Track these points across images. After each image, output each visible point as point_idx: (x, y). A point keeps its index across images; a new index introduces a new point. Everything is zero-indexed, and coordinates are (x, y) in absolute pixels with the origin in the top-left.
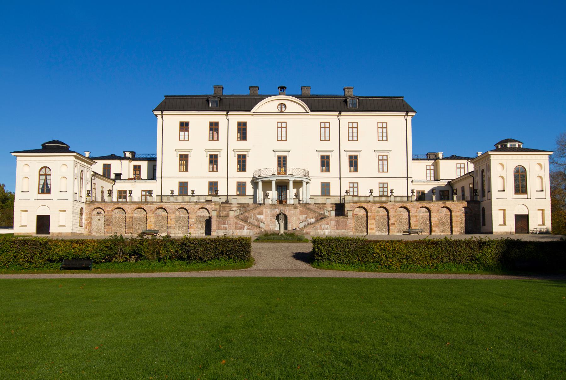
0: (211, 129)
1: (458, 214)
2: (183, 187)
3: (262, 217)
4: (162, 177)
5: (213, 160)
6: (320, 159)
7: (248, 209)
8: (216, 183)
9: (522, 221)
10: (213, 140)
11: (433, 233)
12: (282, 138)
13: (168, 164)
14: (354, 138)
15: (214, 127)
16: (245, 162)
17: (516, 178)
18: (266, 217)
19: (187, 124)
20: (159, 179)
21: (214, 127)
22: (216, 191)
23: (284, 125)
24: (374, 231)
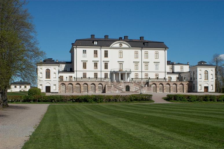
0: (95, 53)
1: (185, 86)
2: (85, 75)
3: (121, 87)
4: (101, 71)
5: (96, 65)
6: (82, 64)
8: (97, 73)
11: (178, 92)
12: (121, 57)
13: (78, 65)
14: (147, 57)
15: (96, 52)
17: (46, 72)
19: (85, 51)
21: (96, 52)
24: (158, 92)
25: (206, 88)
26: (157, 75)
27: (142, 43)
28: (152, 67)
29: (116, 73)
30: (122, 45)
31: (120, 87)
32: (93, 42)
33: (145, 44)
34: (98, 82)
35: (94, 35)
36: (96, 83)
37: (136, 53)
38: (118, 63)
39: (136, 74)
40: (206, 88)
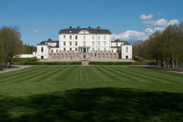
0: (70, 37)
5: (71, 43)
8: (71, 48)
10: (70, 39)
13: (61, 44)
14: (99, 39)
15: (71, 37)
16: (76, 44)
17: (42, 49)
19: (65, 36)
20: (60, 47)
21: (71, 37)
22: (71, 49)
25: (127, 57)
26: (105, 49)
27: (97, 31)
28: (102, 44)
29: (81, 48)
30: (85, 32)
31: (81, 56)
32: (69, 31)
33: (98, 31)
34: (69, 53)
35: (90, 27)
36: (64, 54)
37: (93, 37)
38: (69, 42)
40: (127, 57)
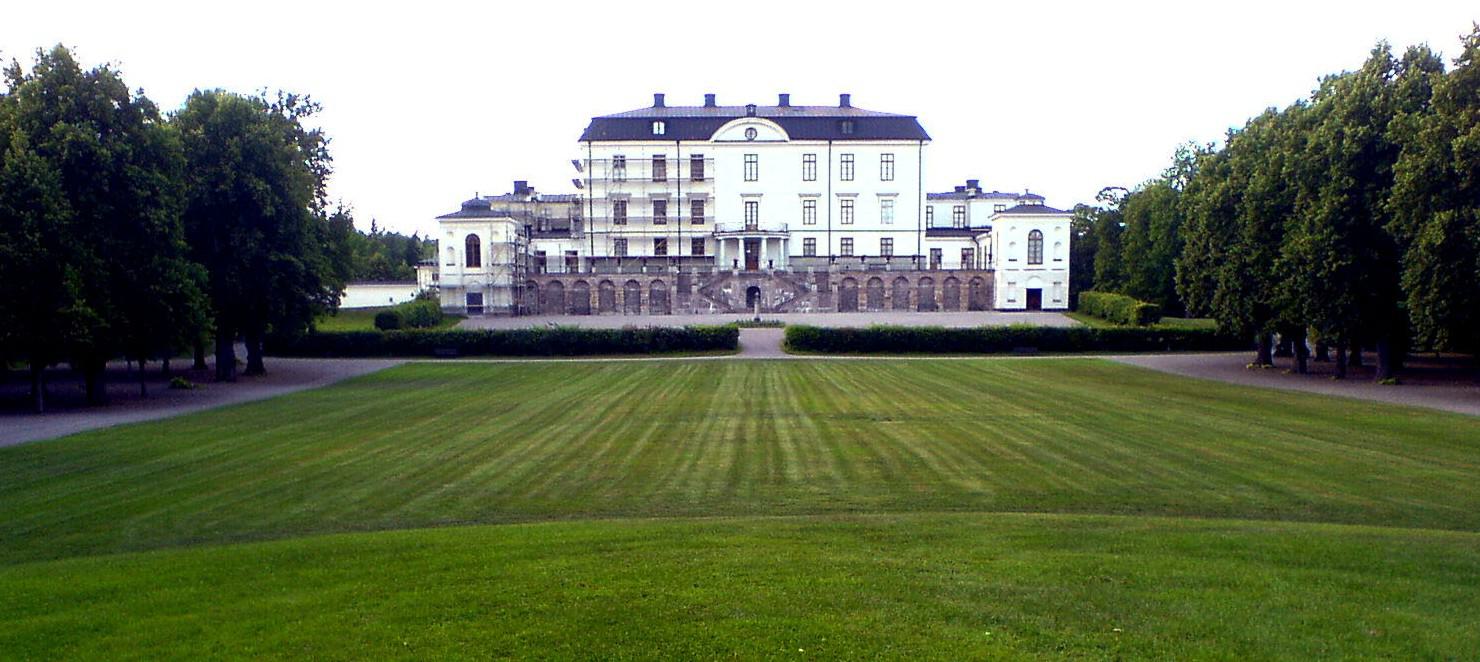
7: (713, 280)
9: (1034, 297)
18: (734, 290)
23: (890, 158)
38: (876, 197)
39: (884, 242)
